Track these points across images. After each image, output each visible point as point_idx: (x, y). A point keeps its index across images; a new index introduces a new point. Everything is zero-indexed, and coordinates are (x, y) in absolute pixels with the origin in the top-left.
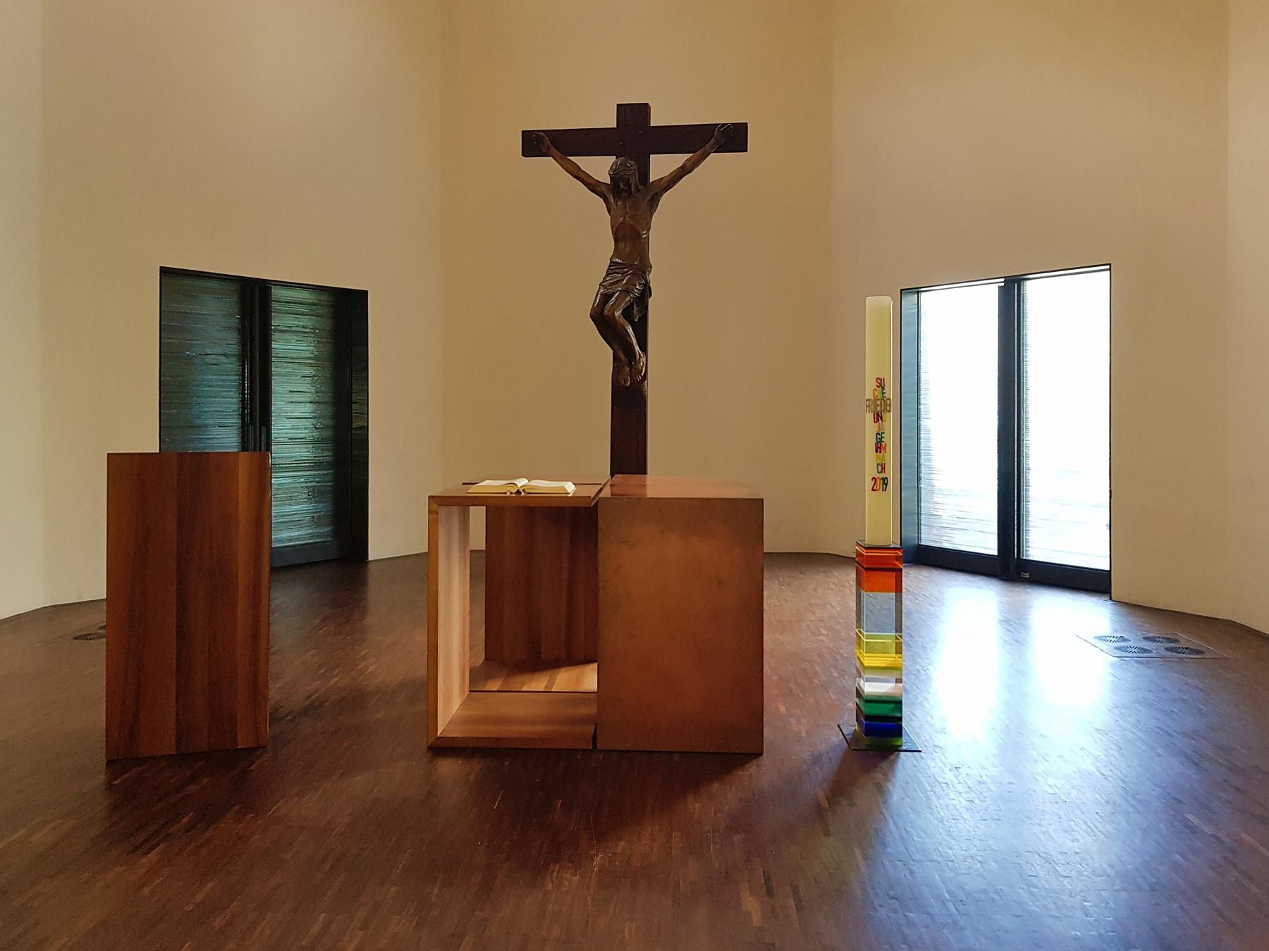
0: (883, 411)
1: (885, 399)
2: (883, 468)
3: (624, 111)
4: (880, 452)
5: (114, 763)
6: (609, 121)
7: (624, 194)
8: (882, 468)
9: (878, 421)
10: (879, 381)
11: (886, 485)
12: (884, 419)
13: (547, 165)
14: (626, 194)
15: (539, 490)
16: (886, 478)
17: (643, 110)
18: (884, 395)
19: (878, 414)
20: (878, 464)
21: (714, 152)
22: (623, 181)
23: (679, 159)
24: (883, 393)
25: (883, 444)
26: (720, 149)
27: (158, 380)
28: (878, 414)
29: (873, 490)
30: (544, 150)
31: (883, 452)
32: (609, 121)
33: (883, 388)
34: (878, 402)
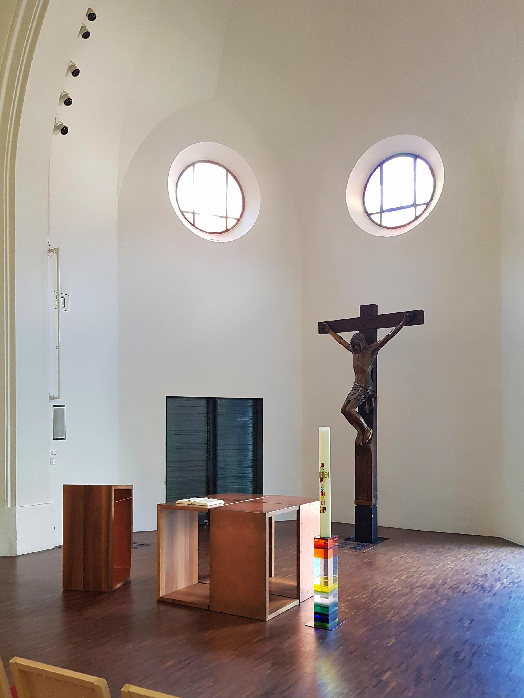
0: (323, 477)
1: (324, 472)
2: (324, 503)
3: (364, 309)
4: (322, 496)
5: (65, 591)
6: (356, 314)
7: (359, 351)
8: (323, 503)
9: (321, 482)
10: (322, 464)
11: (325, 510)
12: (324, 481)
13: (328, 337)
14: (359, 351)
15: (198, 503)
16: (325, 507)
17: (373, 308)
18: (324, 470)
19: (321, 479)
20: (322, 501)
21: (404, 326)
22: (356, 345)
23: (389, 330)
24: (323, 470)
25: (324, 492)
26: (408, 324)
27: (420, 222)
28: (321, 479)
29: (321, 512)
30: (327, 331)
31: (323, 496)
32: (356, 314)
33: (323, 467)
34: (321, 474)
